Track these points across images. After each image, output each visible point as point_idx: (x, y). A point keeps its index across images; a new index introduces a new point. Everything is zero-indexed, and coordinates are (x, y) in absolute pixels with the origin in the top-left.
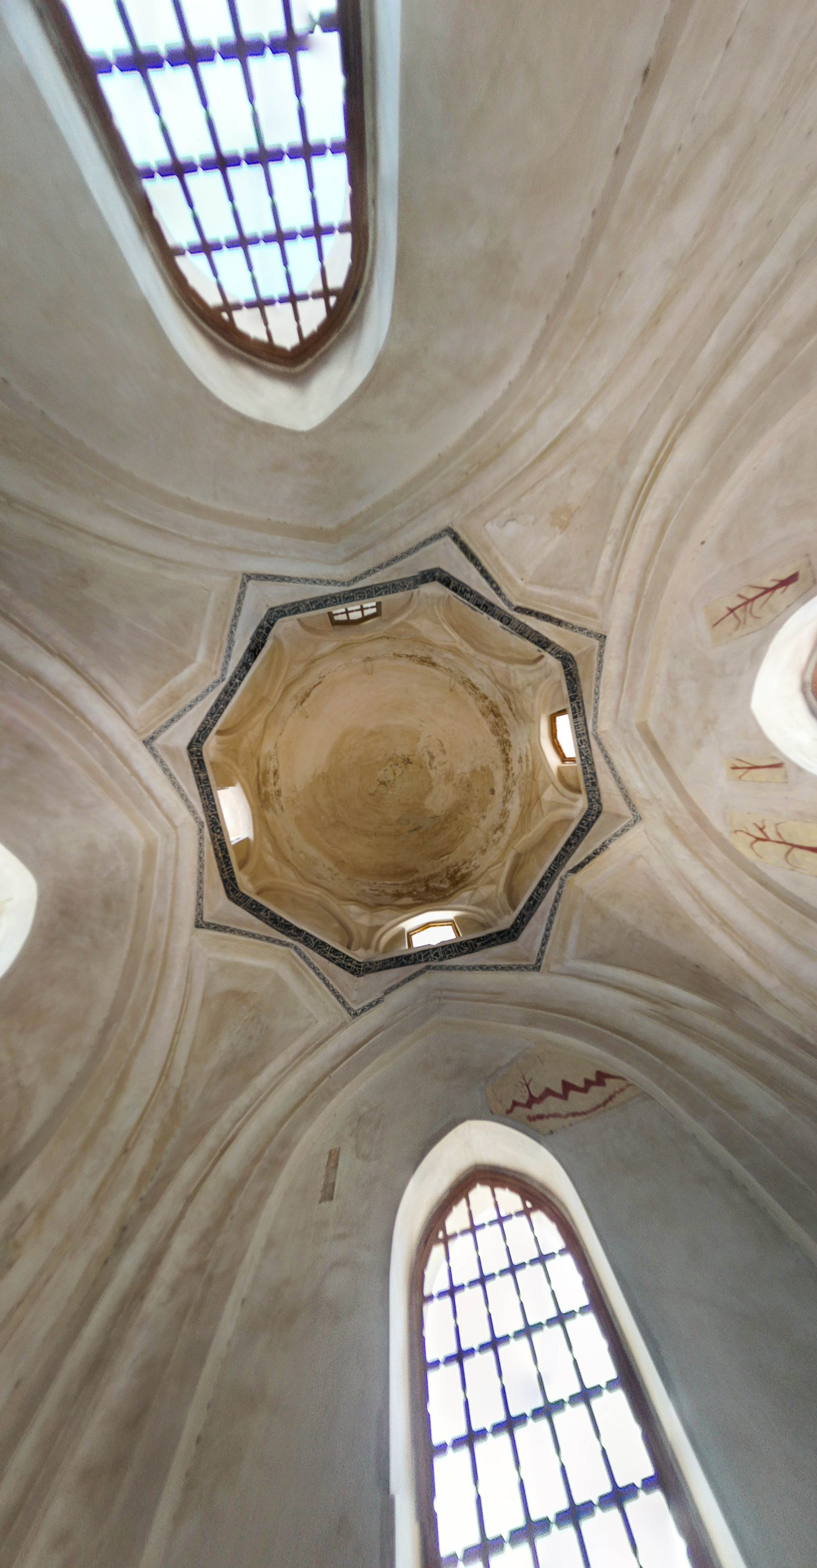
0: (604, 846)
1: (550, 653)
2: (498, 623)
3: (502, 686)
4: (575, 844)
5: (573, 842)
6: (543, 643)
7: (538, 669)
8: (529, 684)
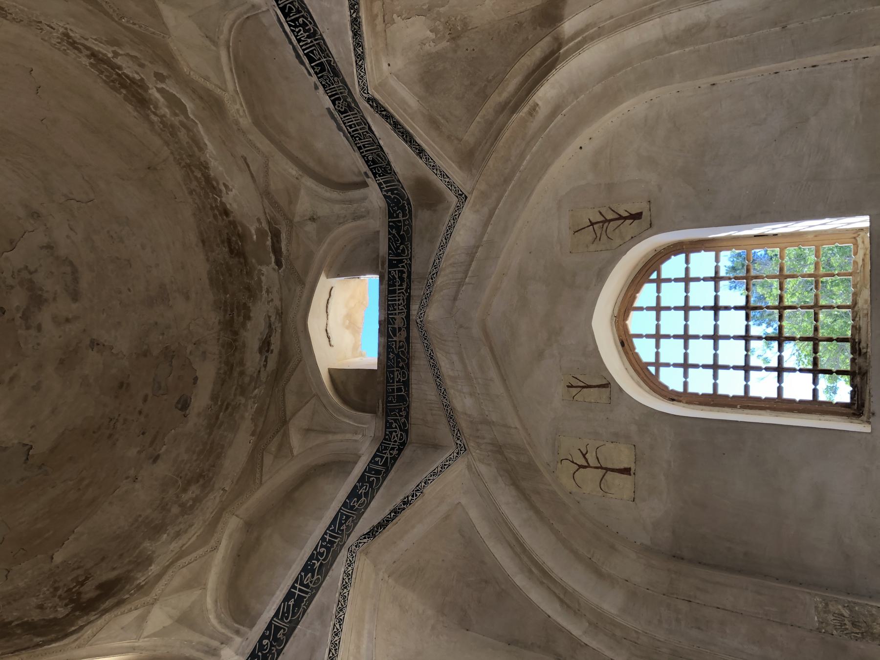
0: (418, 491)
1: (380, 184)
2: (328, 103)
3: (274, 204)
4: (366, 495)
5: (362, 491)
6: (378, 164)
7: (343, 202)
8: (313, 219)
